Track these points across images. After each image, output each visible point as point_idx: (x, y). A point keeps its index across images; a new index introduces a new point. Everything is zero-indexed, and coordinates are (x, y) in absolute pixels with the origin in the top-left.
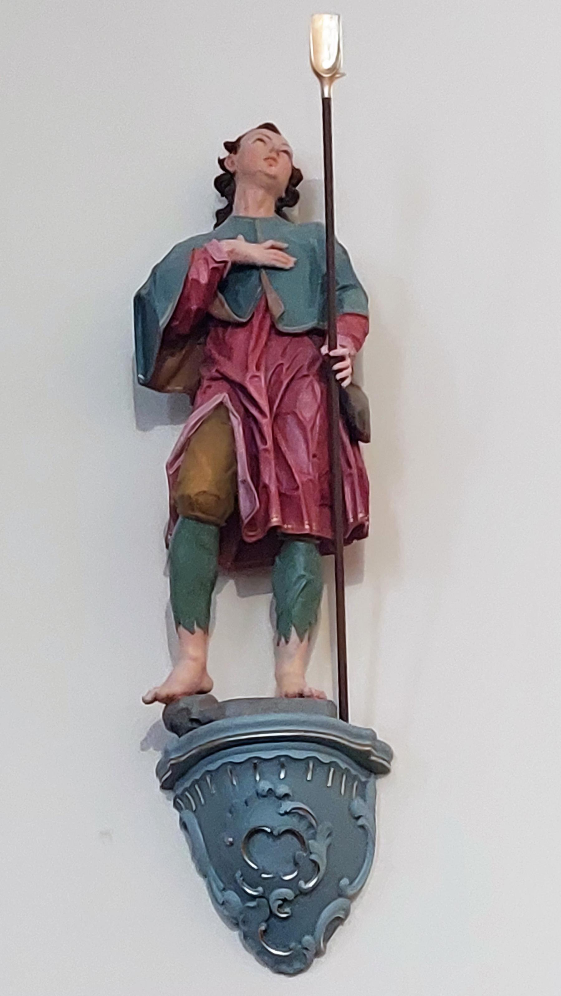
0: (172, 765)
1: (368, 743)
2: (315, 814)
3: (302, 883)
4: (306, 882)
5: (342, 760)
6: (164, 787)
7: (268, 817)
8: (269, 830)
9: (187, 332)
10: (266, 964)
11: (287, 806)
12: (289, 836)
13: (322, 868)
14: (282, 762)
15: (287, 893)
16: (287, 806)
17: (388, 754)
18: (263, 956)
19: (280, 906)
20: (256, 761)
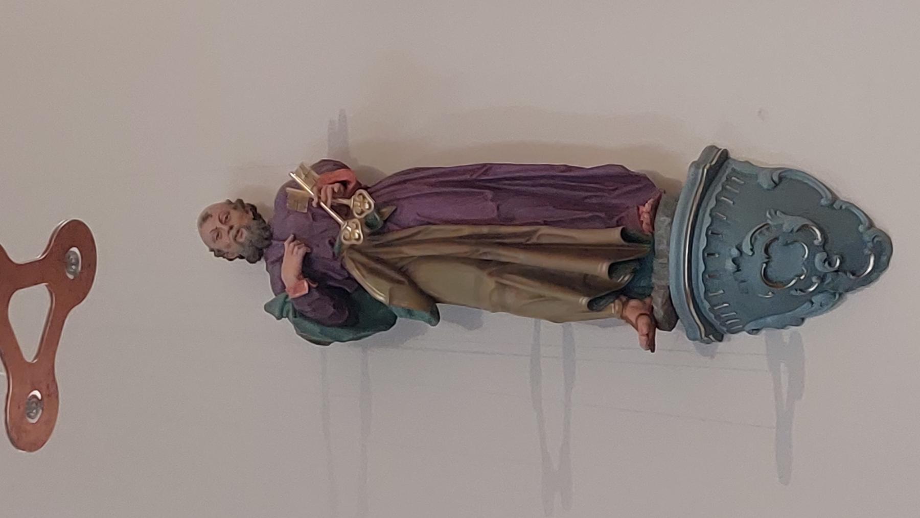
0: (706, 336)
1: (701, 171)
2: (747, 233)
3: (816, 242)
4: (816, 238)
5: (714, 190)
6: (720, 339)
7: (753, 268)
8: (764, 265)
9: (336, 307)
10: (877, 278)
11: (746, 248)
12: (770, 251)
13: (807, 222)
14: (712, 234)
15: (819, 257)
16: (746, 248)
17: (712, 149)
18: (869, 280)
19: (830, 264)
20: (710, 232)
